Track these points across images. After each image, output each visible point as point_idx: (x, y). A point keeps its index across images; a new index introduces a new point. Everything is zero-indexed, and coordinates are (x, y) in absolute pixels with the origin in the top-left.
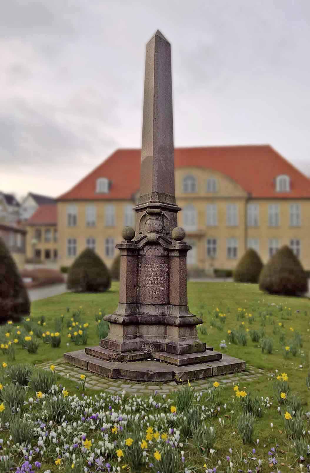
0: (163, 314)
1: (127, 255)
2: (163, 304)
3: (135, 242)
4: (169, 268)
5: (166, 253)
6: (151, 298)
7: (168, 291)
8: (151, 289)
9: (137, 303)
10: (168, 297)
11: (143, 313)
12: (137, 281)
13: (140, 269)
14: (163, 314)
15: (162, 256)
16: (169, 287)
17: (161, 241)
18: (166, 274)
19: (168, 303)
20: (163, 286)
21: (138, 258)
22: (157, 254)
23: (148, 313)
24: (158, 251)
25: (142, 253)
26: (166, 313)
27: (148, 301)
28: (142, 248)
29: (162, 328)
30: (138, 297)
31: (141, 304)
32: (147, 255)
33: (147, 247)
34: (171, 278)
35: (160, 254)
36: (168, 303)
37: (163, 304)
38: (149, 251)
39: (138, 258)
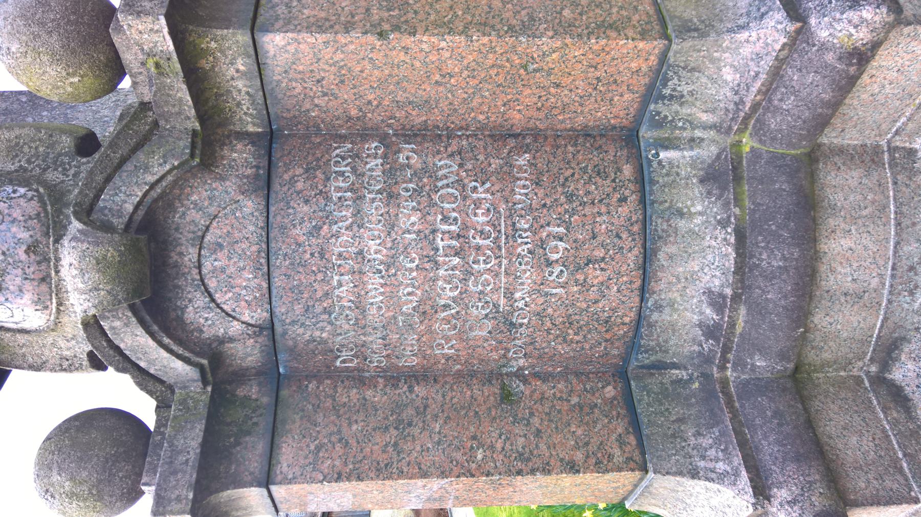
0: (723, 176)
1: (266, 481)
2: (641, 180)
3: (162, 407)
4: (361, 132)
5: (240, 156)
6: (595, 275)
7: (537, 134)
8: (528, 277)
9: (622, 375)
10: (587, 135)
11: (711, 331)
12: (467, 376)
13: (377, 360)
14: (723, 176)
15: (264, 184)
16: (503, 136)
17: (125, 197)
18: (408, 154)
19: (629, 137)
20: (507, 175)
21: (298, 378)
22: (252, 229)
23: (717, 301)
24: (221, 226)
25: (247, 353)
26: (708, 152)
27: (618, 301)
28: (212, 360)
29: (841, 186)
30: (575, 371)
31: (633, 345)
32: (258, 315)
33: (197, 313)
34: (436, 117)
35: (250, 206)
36: (629, 137)
37: (641, 180)
38: (228, 299)
39: (298, 378)
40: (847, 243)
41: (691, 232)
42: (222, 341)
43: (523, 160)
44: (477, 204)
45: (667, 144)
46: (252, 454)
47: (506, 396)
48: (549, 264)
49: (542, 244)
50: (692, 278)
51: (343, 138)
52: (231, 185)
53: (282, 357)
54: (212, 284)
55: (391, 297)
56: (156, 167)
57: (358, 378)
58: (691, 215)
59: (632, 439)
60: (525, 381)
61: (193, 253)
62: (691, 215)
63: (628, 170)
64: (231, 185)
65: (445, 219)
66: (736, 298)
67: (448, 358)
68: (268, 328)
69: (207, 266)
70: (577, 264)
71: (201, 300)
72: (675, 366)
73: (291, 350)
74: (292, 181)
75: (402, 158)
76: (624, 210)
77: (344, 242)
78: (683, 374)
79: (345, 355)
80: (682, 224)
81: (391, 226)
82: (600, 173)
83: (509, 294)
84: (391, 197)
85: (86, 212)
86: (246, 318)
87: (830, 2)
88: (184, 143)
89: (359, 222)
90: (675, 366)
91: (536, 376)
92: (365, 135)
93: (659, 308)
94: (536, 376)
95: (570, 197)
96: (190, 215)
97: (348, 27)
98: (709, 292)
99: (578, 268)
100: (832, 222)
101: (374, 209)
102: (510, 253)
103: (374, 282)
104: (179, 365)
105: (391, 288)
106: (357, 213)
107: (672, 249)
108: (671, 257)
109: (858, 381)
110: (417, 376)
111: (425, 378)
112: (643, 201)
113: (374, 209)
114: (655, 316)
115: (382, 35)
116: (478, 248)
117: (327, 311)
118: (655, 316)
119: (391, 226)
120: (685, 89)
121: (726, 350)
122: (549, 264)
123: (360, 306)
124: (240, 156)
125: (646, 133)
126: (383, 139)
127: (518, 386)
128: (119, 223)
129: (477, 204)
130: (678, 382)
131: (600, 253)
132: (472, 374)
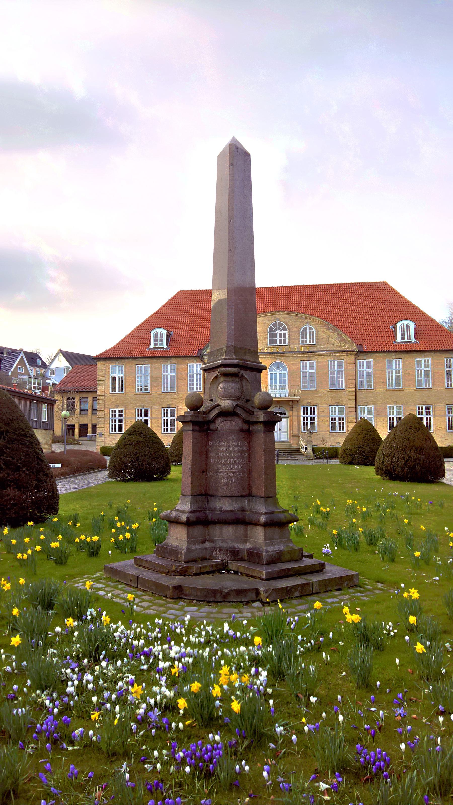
0: (243, 510)
2: (242, 496)
5: (246, 427)
6: (225, 487)
8: (225, 475)
10: (250, 486)
12: (206, 464)
13: (210, 448)
15: (241, 430)
16: (250, 472)
17: (239, 411)
18: (247, 454)
20: (243, 472)
25: (212, 427)
26: (247, 507)
27: (221, 491)
31: (211, 496)
32: (219, 429)
35: (238, 428)
36: (250, 495)
37: (242, 496)
38: (222, 425)
39: (207, 435)
40: (231, 531)
41: (233, 504)
42: (215, 423)
43: (246, 475)
44: (238, 466)
45: (249, 501)
46: (196, 428)
47: (203, 472)
48: (227, 479)
49: (231, 478)
50: (225, 505)
51: (249, 444)
52: (241, 425)
53: (212, 432)
54: (225, 422)
55: (222, 451)
56: (243, 415)
57: (207, 445)
58: (236, 504)
59: (196, 494)
60: (206, 476)
61: (230, 419)
62: (236, 504)
63: (244, 494)
64: (241, 425)
65: (235, 461)
66: (222, 511)
67: (210, 461)
68: (217, 430)
69: (228, 421)
70: (227, 484)
71: (222, 420)
72: (208, 504)
73: (213, 434)
74: (242, 435)
75: (246, 453)
76: (237, 493)
77: (231, 443)
78: (206, 505)
79: (212, 443)
80: (234, 503)
81: (234, 451)
82: (243, 489)
83: (222, 472)
84: (239, 451)
85: (237, 405)
86: (219, 427)
87: (400, 804)
88: (247, 419)
89: (235, 446)
90: (208, 504)
91: (206, 478)
92: (250, 447)
93: (219, 499)
94: (206, 478)
95: (239, 483)
96: (236, 419)
97: (265, 446)
98: (222, 507)
99: (227, 484)
100: (234, 528)
101: (237, 449)
102: (229, 472)
103: (224, 448)
104: (212, 417)
105: (224, 451)
106: (237, 446)
107: (230, 501)
108: (228, 501)
109: (206, 537)
110: (207, 455)
111: (206, 457)
112: (238, 496)
113: (237, 449)
114: (218, 499)
115: (264, 450)
116: (230, 466)
117: (220, 441)
118: (218, 499)
119: (234, 451)
120: (257, 502)
121: (212, 510)
122: (227, 479)
123: (220, 446)
124: (246, 427)
125: (250, 498)
126: (249, 450)
127: (204, 474)
128: (235, 410)
129: (238, 466)
130: (205, 504)
131: (229, 488)
132: (207, 466)
